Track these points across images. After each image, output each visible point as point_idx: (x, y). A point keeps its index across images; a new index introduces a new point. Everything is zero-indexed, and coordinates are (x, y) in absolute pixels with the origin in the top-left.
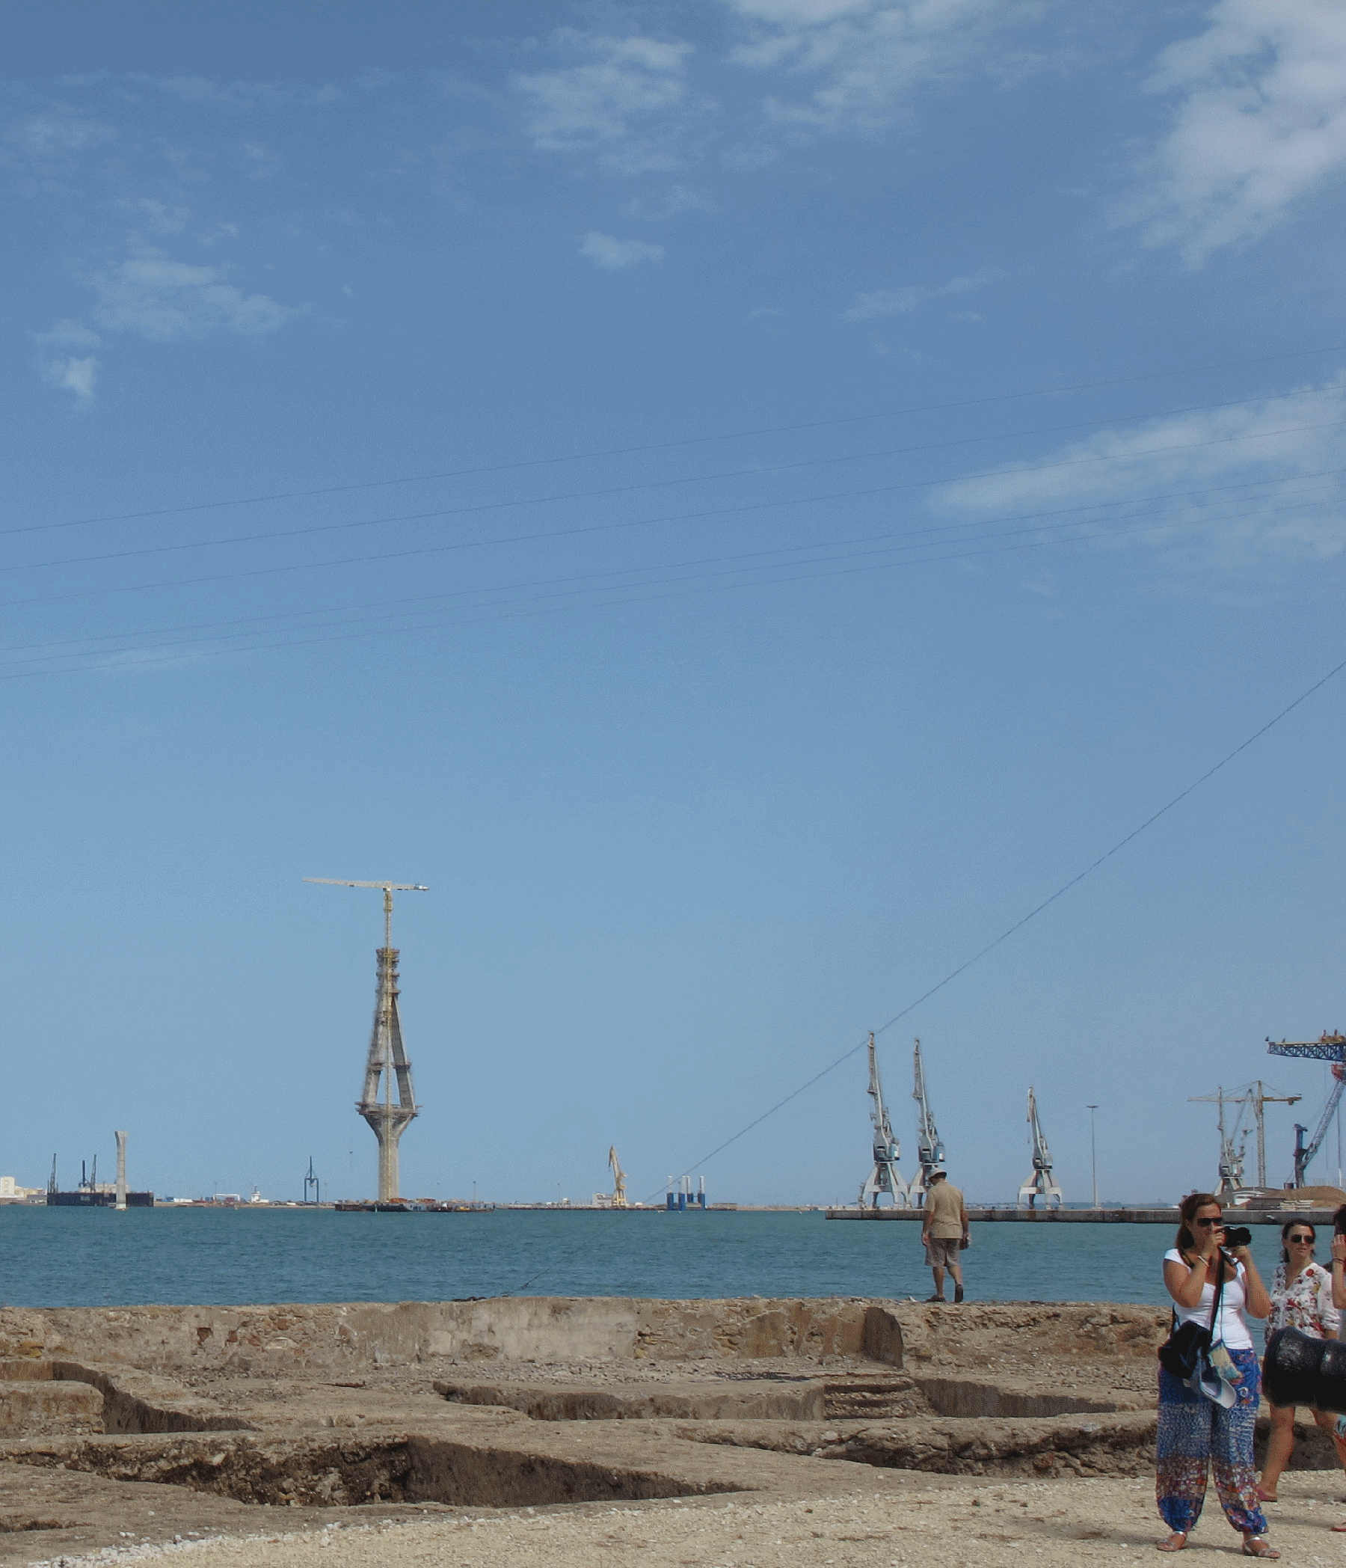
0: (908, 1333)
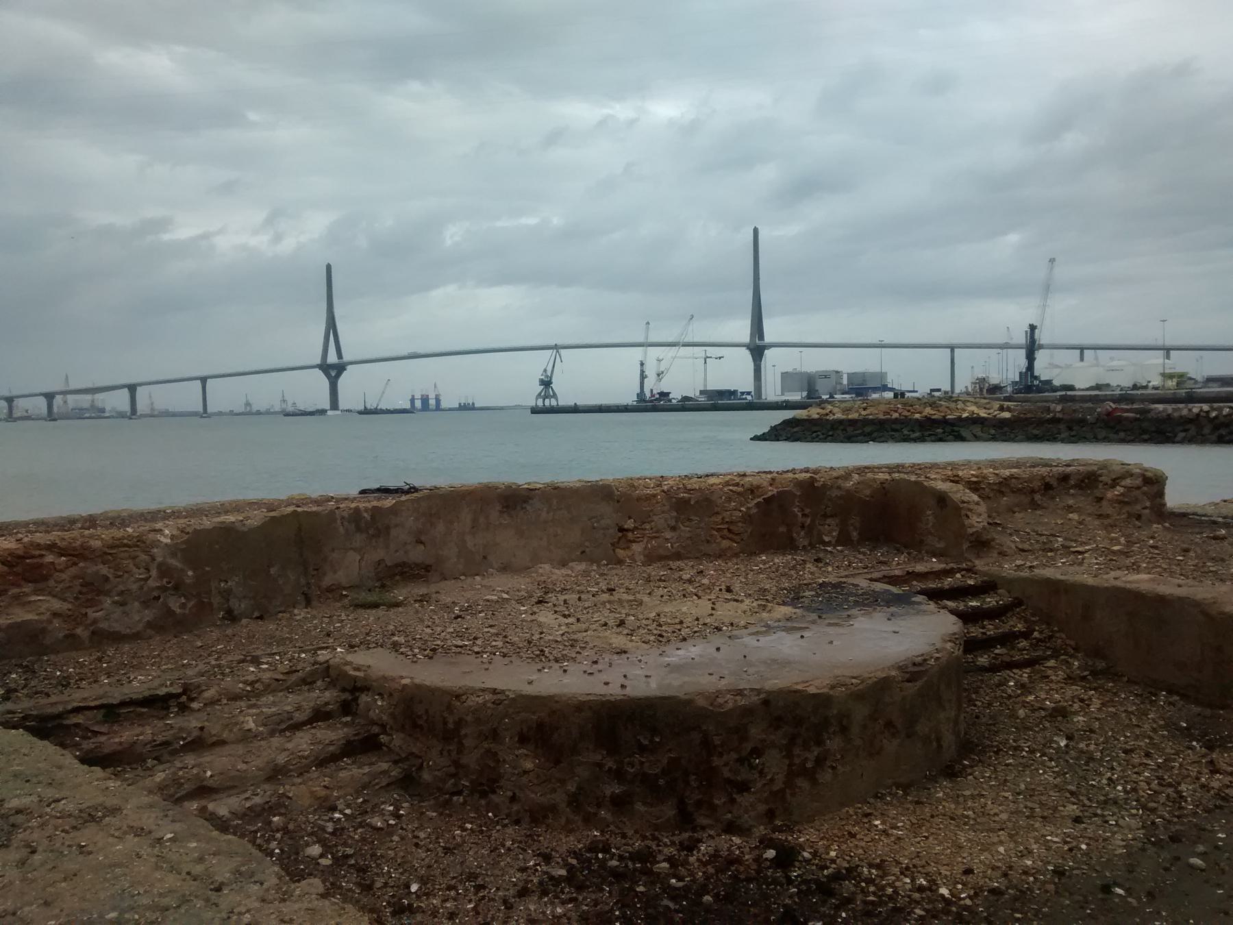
0: (969, 513)
